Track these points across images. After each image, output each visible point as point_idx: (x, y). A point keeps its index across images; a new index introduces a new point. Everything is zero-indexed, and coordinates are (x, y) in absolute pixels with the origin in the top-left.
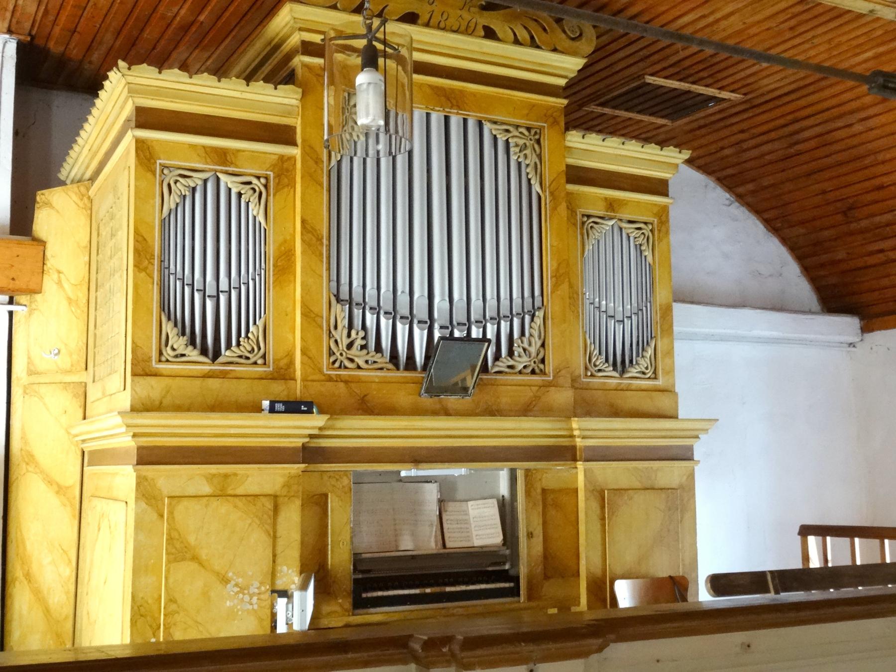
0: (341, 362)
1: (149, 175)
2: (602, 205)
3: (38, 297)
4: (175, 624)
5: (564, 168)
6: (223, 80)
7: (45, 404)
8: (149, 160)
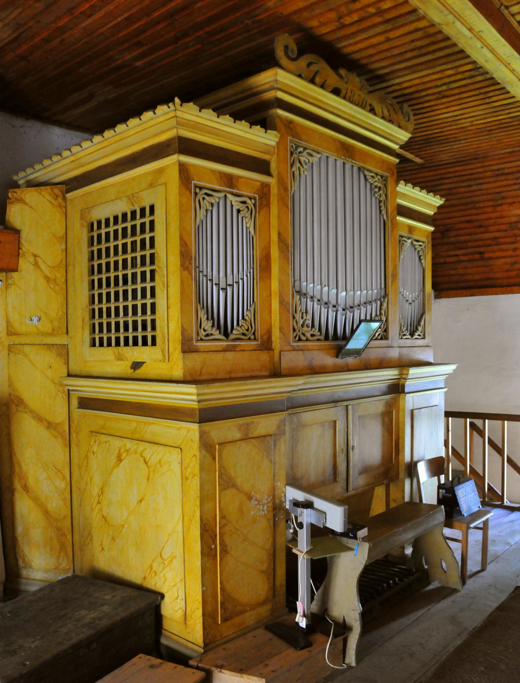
0: (299, 336)
1: (188, 192)
2: (407, 229)
3: (14, 274)
4: (225, 533)
5: (396, 205)
6: (237, 121)
7: (30, 360)
8: (187, 181)
